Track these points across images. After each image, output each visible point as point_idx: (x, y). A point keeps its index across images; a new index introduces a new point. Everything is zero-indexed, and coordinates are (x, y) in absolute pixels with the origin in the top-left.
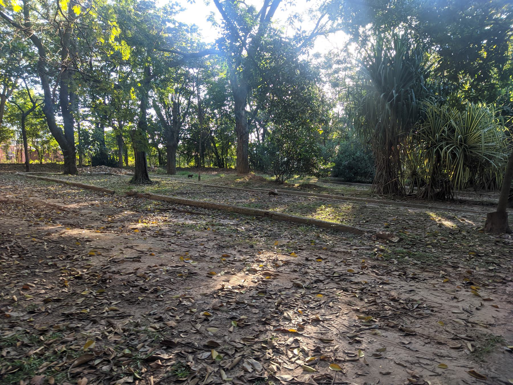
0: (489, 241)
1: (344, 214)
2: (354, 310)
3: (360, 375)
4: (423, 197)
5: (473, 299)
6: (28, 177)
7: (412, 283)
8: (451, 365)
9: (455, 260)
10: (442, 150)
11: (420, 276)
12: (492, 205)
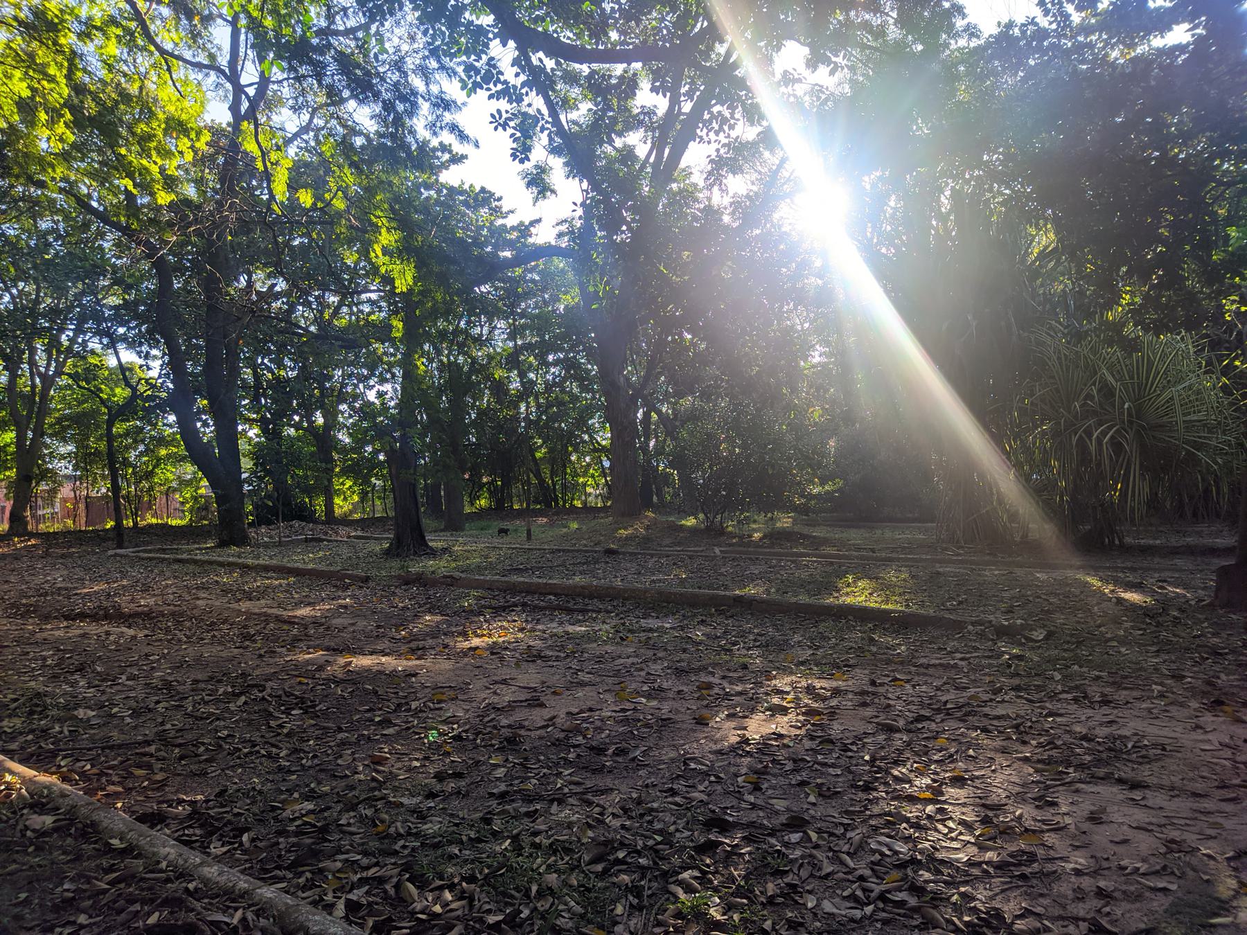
1: (901, 590)
2: (1019, 759)
3: (1078, 847)
5: (1232, 728)
6: (143, 559)
7: (1105, 710)
8: (1228, 824)
9: (1174, 666)
11: (1116, 697)
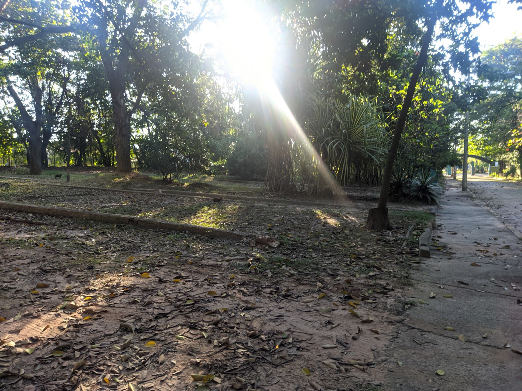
0: (371, 240)
4: (312, 194)
5: (350, 322)
10: (328, 145)
11: (294, 291)
12: (374, 200)
